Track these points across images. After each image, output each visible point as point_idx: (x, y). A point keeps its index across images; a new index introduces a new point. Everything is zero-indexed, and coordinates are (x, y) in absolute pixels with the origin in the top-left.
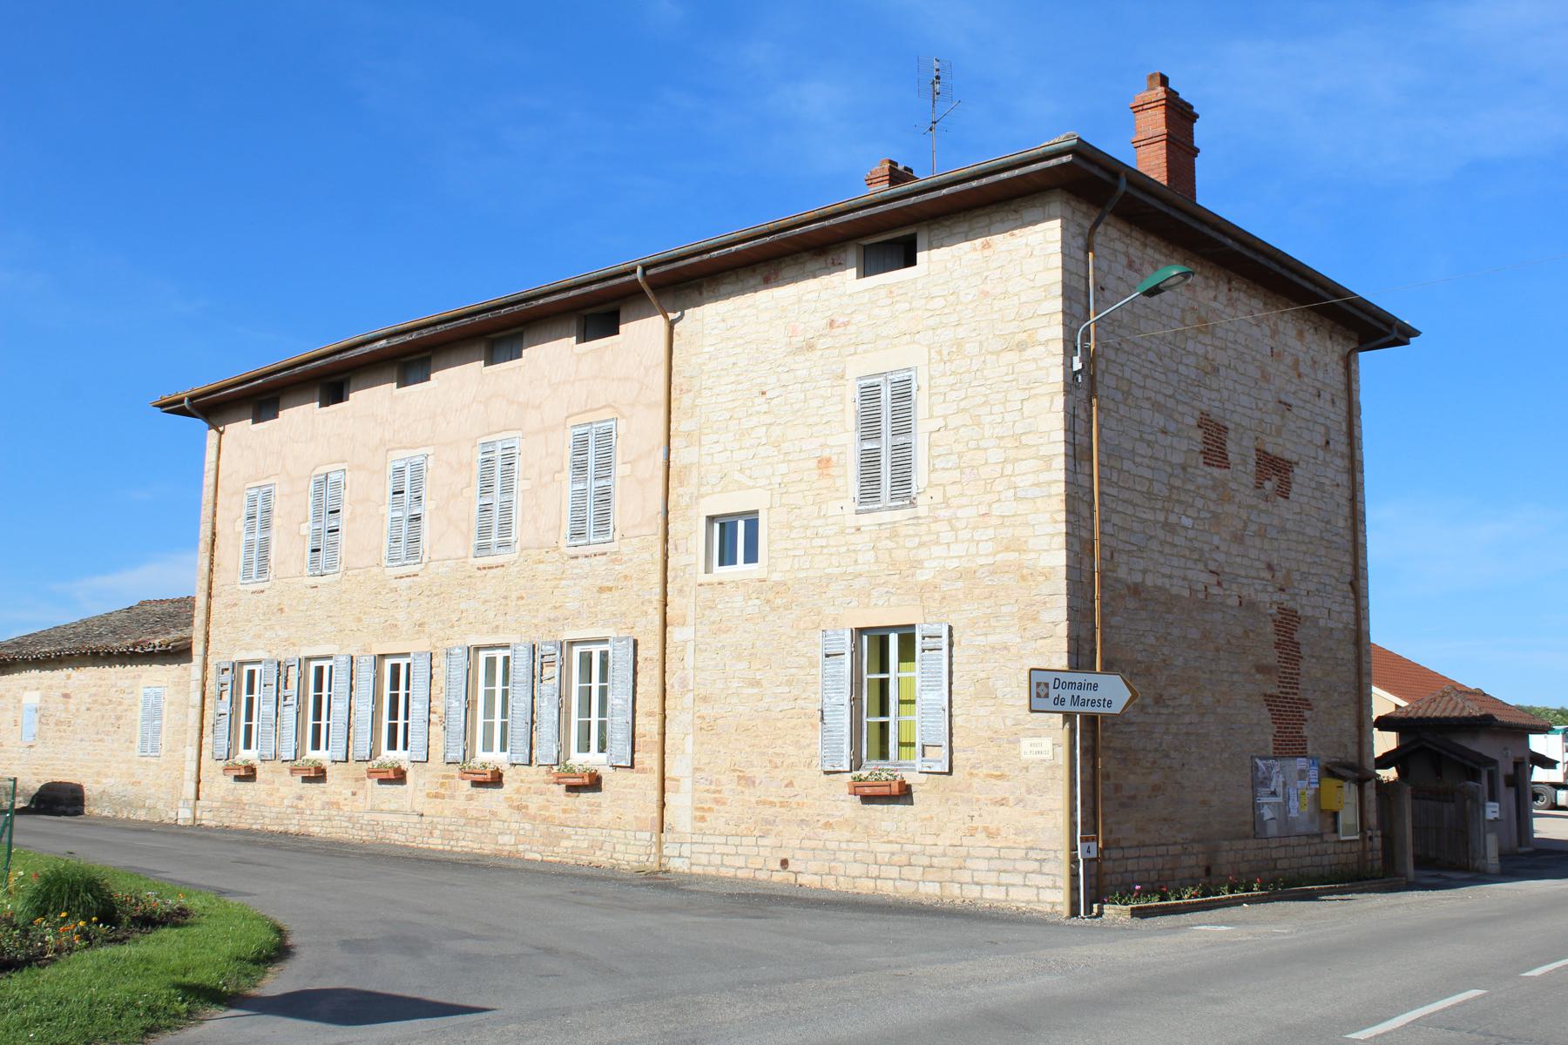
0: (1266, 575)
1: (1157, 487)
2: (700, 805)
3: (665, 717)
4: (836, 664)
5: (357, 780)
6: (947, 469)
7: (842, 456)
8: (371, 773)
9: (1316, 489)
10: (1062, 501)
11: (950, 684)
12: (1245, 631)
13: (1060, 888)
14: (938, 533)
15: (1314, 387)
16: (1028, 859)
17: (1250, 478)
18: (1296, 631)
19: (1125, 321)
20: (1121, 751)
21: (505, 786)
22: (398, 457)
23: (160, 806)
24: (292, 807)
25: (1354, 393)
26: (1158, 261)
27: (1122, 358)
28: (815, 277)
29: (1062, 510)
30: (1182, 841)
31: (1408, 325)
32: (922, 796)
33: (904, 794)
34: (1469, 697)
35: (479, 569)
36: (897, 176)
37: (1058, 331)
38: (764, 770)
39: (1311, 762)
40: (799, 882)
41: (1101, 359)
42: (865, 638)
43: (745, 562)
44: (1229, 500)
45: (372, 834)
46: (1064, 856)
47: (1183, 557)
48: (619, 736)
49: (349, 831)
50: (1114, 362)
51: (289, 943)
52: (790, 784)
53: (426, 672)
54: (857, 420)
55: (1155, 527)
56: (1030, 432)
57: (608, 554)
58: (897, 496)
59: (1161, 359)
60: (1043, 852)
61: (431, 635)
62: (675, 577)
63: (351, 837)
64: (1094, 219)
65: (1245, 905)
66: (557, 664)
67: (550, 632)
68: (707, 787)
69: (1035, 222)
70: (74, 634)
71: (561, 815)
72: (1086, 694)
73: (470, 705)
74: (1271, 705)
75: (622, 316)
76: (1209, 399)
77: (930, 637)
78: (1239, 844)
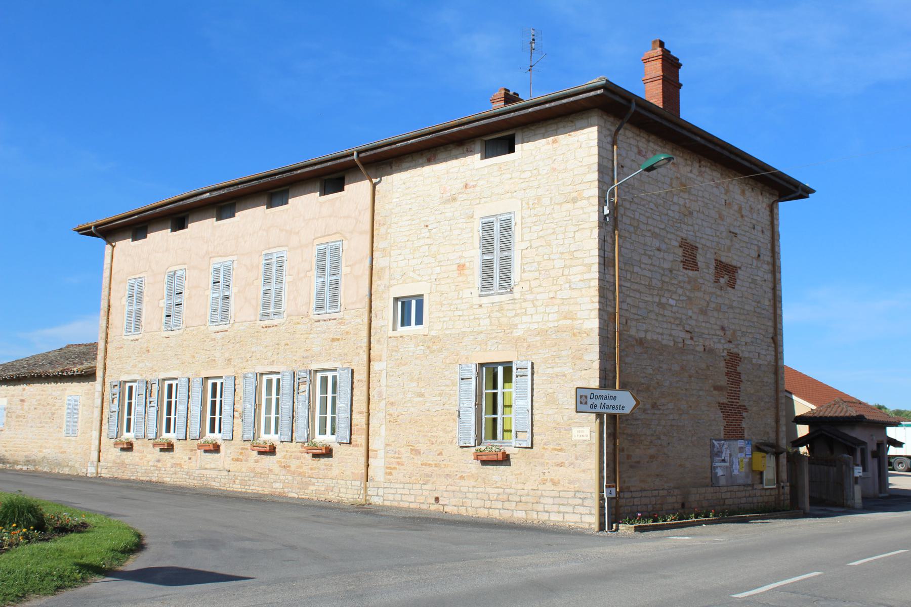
0: (721, 333)
1: (654, 282)
2: (390, 466)
3: (369, 414)
4: (467, 384)
5: (192, 450)
6: (532, 271)
7: (472, 263)
8: (200, 446)
9: (751, 283)
10: (597, 290)
11: (532, 396)
12: (707, 366)
14: (526, 309)
15: (751, 223)
16: (576, 498)
17: (711, 277)
18: (739, 366)
19: (636, 185)
20: (631, 435)
21: (277, 454)
22: (217, 262)
23: (77, 465)
24: (154, 466)
25: (775, 226)
26: (656, 150)
27: (634, 207)
28: (457, 159)
29: (596, 296)
30: (667, 488)
31: (808, 187)
32: (516, 461)
33: (505, 460)
34: (850, 404)
35: (263, 327)
36: (509, 98)
37: (594, 191)
38: (425, 446)
39: (747, 442)
40: (445, 510)
41: (621, 208)
42: (484, 369)
43: (416, 324)
44: (698, 289)
45: (200, 482)
46: (596, 496)
47: (670, 322)
48: (343, 426)
49: (187, 480)
50: (629, 209)
51: (144, 542)
53: (232, 387)
54: (480, 243)
55: (653, 305)
56: (579, 250)
57: (337, 319)
58: (503, 287)
59: (657, 208)
60: (585, 494)
61: (235, 366)
62: (376, 333)
63: (188, 484)
64: (617, 126)
65: (704, 525)
66: (307, 383)
67: (303, 364)
68: (393, 455)
70: (27, 364)
71: (309, 471)
73: (257, 407)
74: (723, 409)
75: (346, 181)
76: (687, 230)
77: (521, 369)
78: (703, 490)
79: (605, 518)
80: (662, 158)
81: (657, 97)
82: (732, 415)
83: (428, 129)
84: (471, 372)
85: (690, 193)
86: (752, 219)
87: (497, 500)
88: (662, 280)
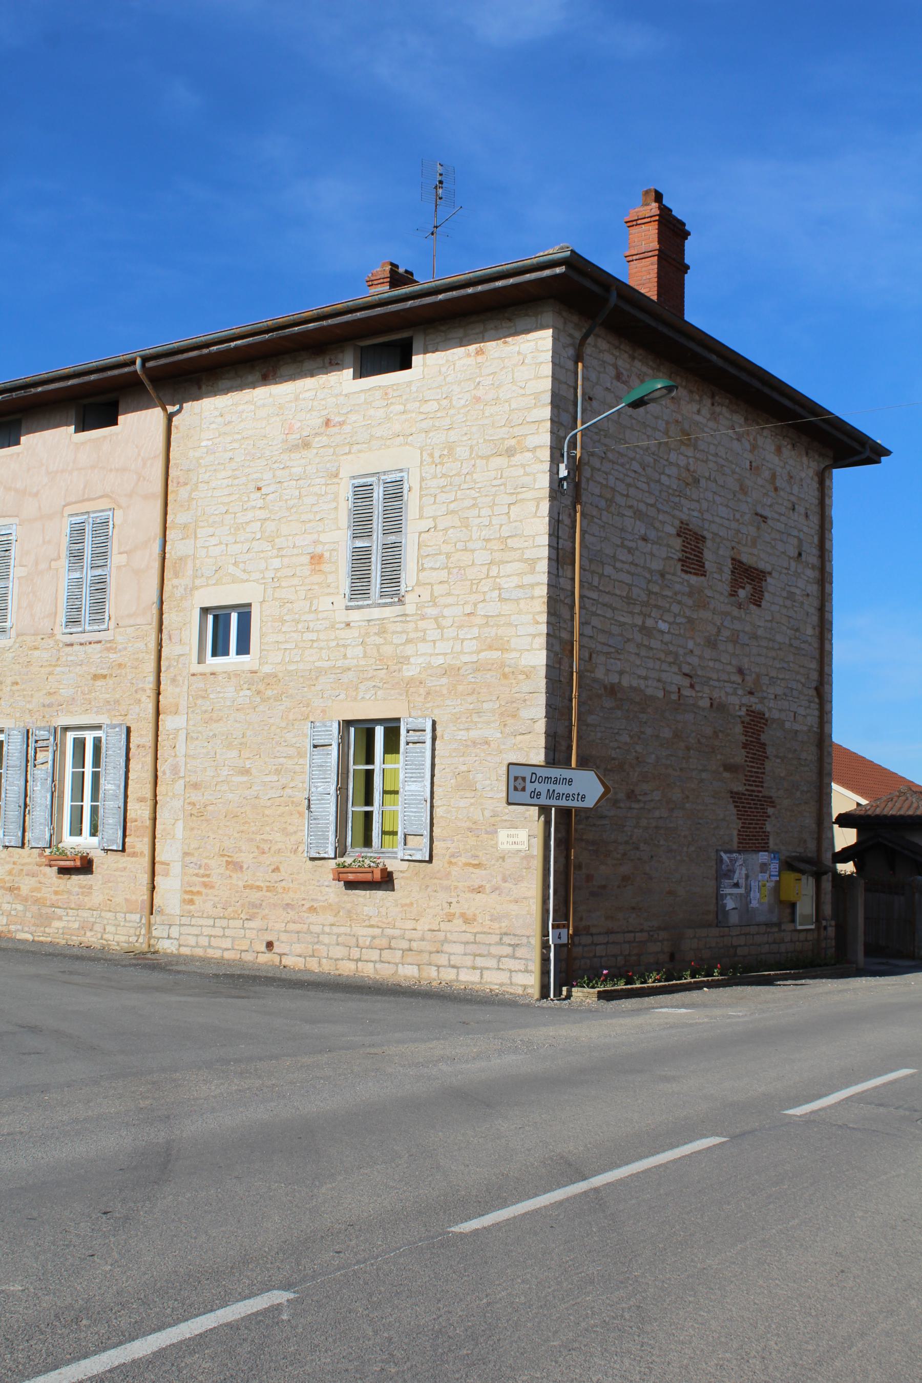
0: (737, 678)
3: (156, 803)
6: (435, 569)
9: (787, 598)
10: (544, 602)
11: (433, 776)
12: (715, 732)
13: (531, 972)
14: (424, 631)
15: (789, 500)
16: (502, 944)
18: (763, 732)
26: (645, 374)
28: (312, 376)
29: (542, 612)
33: (386, 881)
36: (397, 278)
37: (545, 438)
38: (252, 856)
41: (586, 467)
42: (352, 730)
46: (536, 941)
47: (659, 659)
50: (599, 470)
52: (276, 870)
54: (349, 519)
59: (644, 469)
62: (168, 667)
64: (584, 330)
65: (705, 989)
66: (51, 749)
67: (44, 717)
68: (196, 871)
69: (528, 331)
72: (560, 789)
75: (121, 408)
76: (689, 509)
79: (549, 977)
80: (659, 386)
81: (650, 285)
82: (751, 812)
83: (265, 324)
84: (331, 735)
85: (696, 448)
86: (791, 494)
87: (370, 947)
88: (648, 590)
